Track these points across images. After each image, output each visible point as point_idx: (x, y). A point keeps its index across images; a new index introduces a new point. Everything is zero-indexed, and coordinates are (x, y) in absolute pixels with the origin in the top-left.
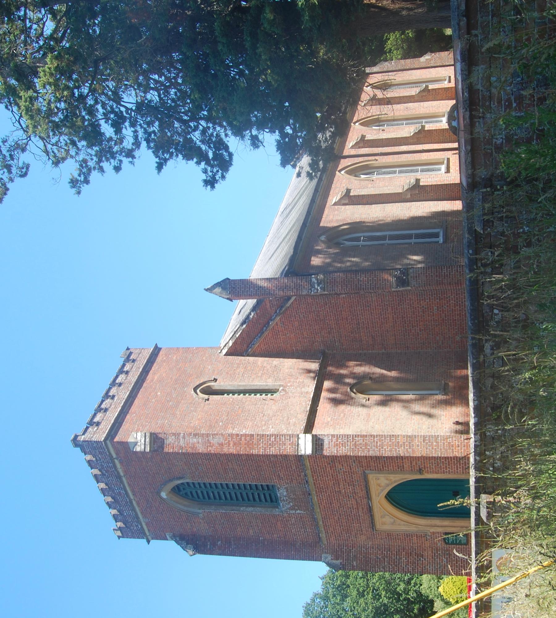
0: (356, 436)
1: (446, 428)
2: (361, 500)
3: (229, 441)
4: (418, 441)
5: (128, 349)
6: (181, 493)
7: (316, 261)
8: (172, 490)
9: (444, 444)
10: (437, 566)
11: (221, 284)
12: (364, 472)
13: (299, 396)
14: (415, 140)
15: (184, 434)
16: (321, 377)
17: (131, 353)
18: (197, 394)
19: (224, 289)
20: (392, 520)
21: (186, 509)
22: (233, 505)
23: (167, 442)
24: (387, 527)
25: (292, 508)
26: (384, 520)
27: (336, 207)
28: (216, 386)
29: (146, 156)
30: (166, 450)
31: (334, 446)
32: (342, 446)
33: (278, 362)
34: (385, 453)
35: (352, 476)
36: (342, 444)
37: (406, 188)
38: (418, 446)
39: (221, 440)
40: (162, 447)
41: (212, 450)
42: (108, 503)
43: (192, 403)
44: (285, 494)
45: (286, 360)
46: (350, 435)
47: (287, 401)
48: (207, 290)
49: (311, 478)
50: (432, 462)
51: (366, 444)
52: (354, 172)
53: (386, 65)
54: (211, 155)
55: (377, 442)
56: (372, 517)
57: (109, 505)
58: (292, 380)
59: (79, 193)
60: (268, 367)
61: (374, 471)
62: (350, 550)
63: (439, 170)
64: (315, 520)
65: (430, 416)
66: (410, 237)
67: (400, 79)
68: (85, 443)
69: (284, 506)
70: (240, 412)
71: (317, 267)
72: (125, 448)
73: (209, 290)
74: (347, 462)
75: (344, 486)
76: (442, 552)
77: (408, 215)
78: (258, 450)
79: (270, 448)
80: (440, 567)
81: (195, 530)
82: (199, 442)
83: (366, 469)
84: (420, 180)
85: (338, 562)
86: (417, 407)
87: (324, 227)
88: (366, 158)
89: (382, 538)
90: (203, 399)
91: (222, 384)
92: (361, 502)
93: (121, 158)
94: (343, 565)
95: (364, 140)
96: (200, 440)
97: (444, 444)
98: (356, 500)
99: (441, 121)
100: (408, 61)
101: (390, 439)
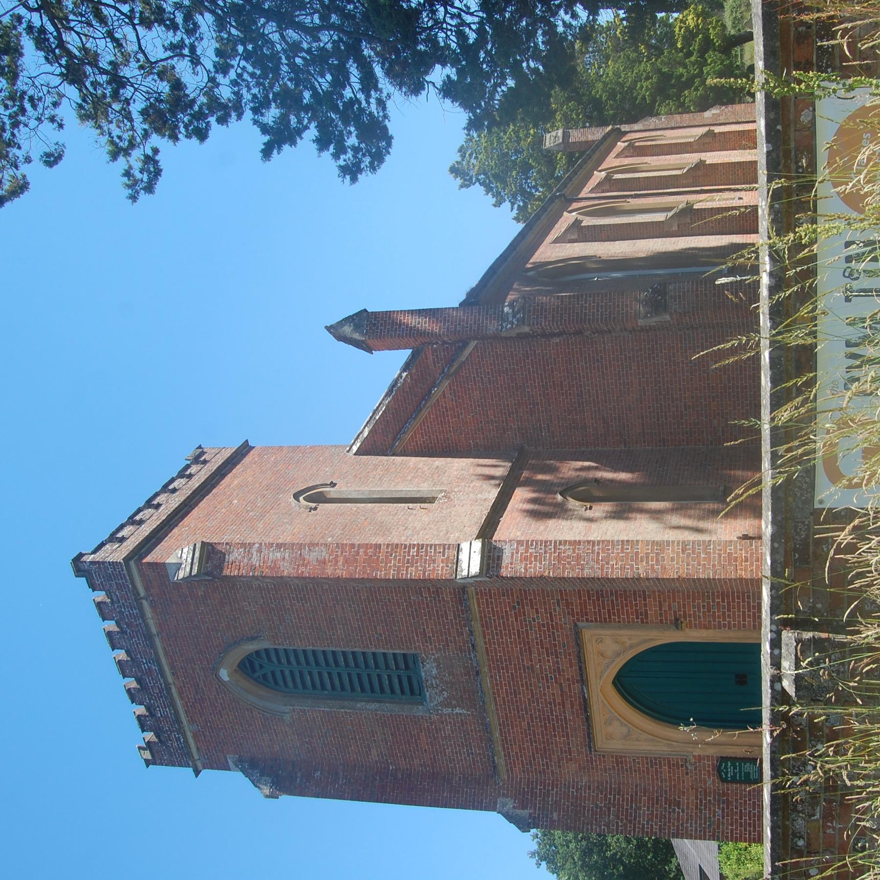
0: (560, 542)
2: (570, 685)
3: (337, 555)
4: (673, 551)
5: (200, 447)
6: (256, 675)
8: (238, 666)
9: (720, 555)
10: (705, 823)
11: (353, 319)
12: (576, 625)
13: (471, 505)
15: (261, 544)
17: (203, 453)
20: (624, 730)
23: (231, 558)
24: (616, 745)
25: (447, 704)
28: (332, 492)
30: (226, 572)
31: (521, 561)
32: (536, 560)
34: (612, 572)
35: (554, 633)
36: (536, 557)
38: (672, 559)
39: (324, 554)
41: (306, 572)
42: (129, 691)
44: (435, 671)
46: (551, 542)
47: (448, 510)
49: (482, 639)
50: (699, 603)
51: (579, 557)
53: (652, 122)
55: (598, 553)
56: (588, 720)
57: (132, 695)
58: (463, 484)
60: (426, 468)
61: (594, 624)
62: (548, 790)
64: (487, 728)
68: (94, 567)
69: (434, 697)
74: (545, 603)
75: (539, 656)
76: (714, 797)
78: (388, 571)
79: (408, 567)
80: (710, 826)
81: (277, 748)
82: (284, 559)
83: (578, 621)
85: (525, 813)
89: (606, 769)
90: (307, 507)
91: (344, 489)
92: (570, 691)
94: (534, 818)
96: (287, 555)
97: (720, 555)
98: (561, 685)
101: (622, 547)
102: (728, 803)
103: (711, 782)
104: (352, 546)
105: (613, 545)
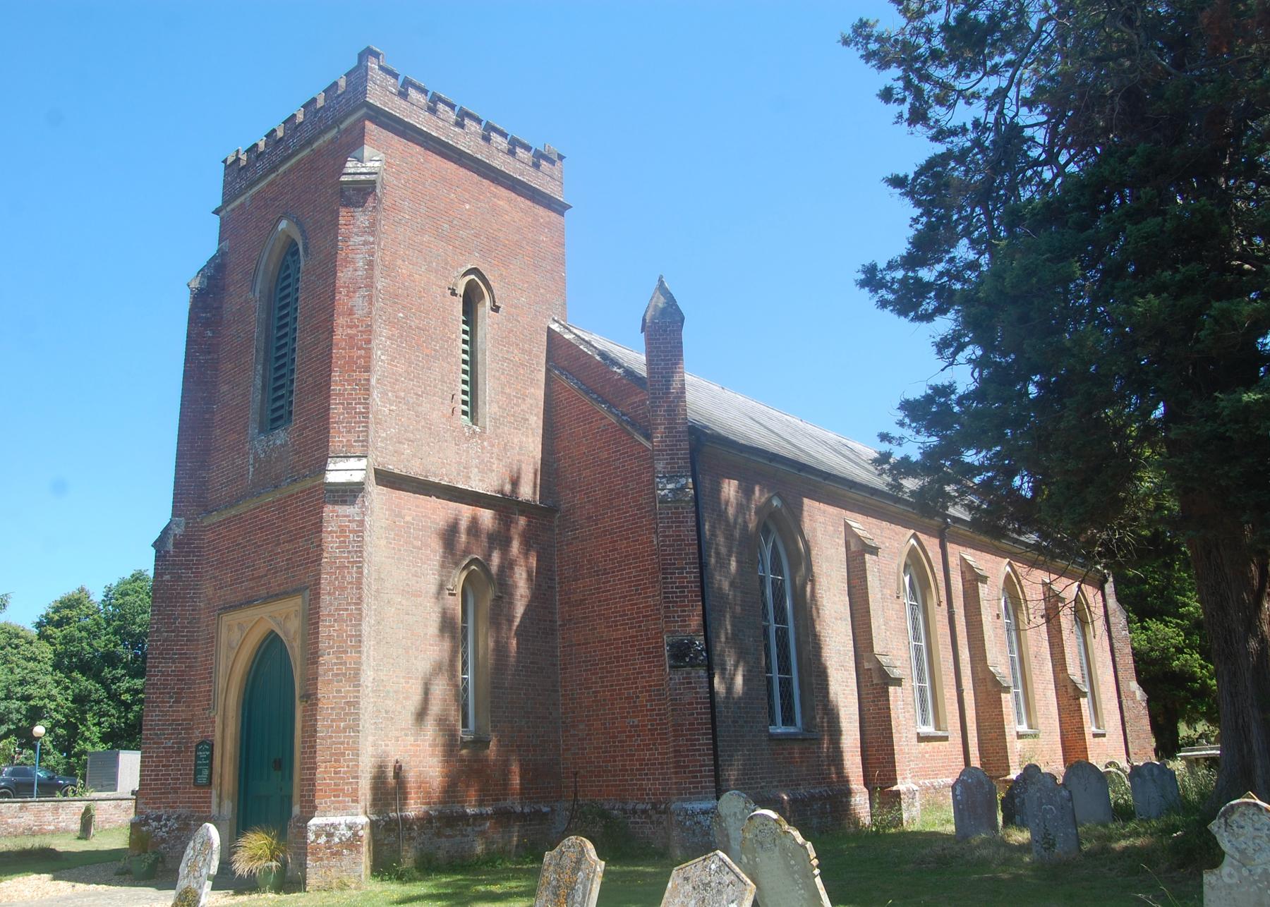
1: (387, 745)
5: (561, 158)
6: (289, 258)
7: (730, 489)
9: (342, 743)
14: (981, 676)
15: (373, 243)
16: (504, 505)
17: (553, 162)
18: (465, 275)
19: (663, 312)
20: (234, 644)
21: (262, 268)
22: (266, 352)
26: (236, 629)
27: (842, 529)
28: (484, 309)
29: (917, 149)
30: (343, 212)
33: (534, 426)
37: (883, 660)
40: (349, 203)
41: (341, 296)
43: (446, 264)
44: (278, 442)
45: (539, 439)
48: (661, 283)
52: (915, 563)
53: (1119, 619)
54: (926, 274)
59: (846, 42)
60: (524, 407)
65: (421, 715)
66: (785, 667)
67: (1095, 646)
70: (428, 352)
71: (717, 490)
72: (353, 144)
73: (897, 182)
77: (828, 664)
78: (339, 383)
84: (900, 685)
86: (440, 689)
87: (801, 505)
88: (942, 585)
90: (455, 284)
93: (909, 100)
95: (977, 580)
97: (342, 743)
99: (1020, 722)
100: (1130, 660)
102: (179, 752)
103: (197, 735)
104: (369, 342)
105: (355, 625)
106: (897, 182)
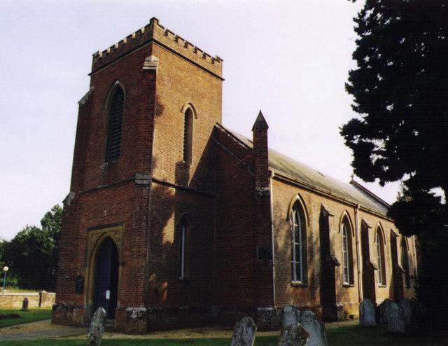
63: (347, 281)
73: (260, 113)
106: (260, 113)
